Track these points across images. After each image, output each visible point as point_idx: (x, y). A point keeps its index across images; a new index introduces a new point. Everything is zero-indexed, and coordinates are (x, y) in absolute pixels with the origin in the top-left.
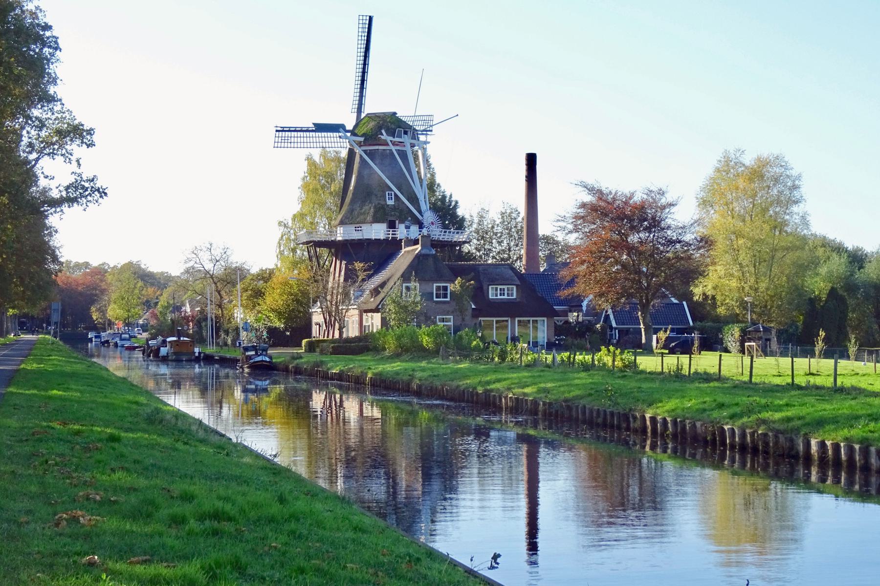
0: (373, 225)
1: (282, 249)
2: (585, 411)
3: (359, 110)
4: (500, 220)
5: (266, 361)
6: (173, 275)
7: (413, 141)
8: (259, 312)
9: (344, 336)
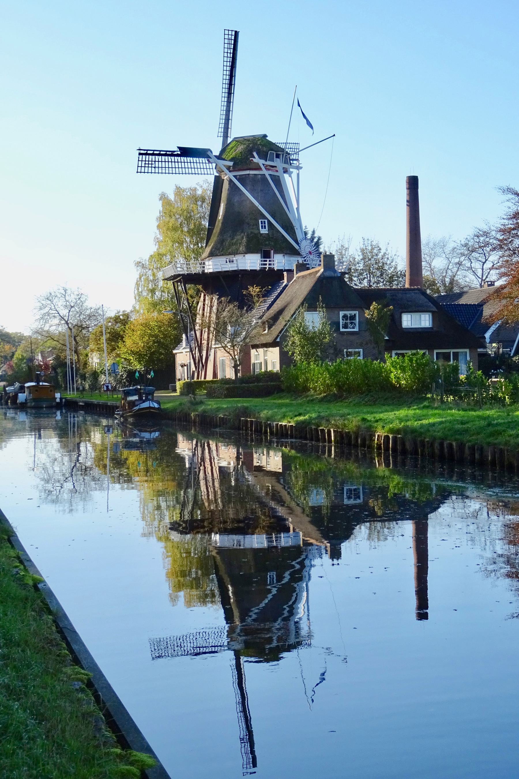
0: (246, 255)
1: (140, 290)
2: (397, 441)
3: (226, 135)
4: (361, 257)
5: (154, 408)
6: (25, 335)
7: (286, 166)
8: (118, 355)
9: (219, 377)
